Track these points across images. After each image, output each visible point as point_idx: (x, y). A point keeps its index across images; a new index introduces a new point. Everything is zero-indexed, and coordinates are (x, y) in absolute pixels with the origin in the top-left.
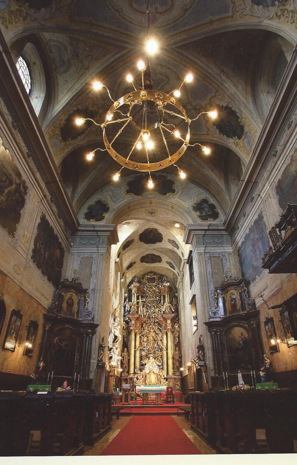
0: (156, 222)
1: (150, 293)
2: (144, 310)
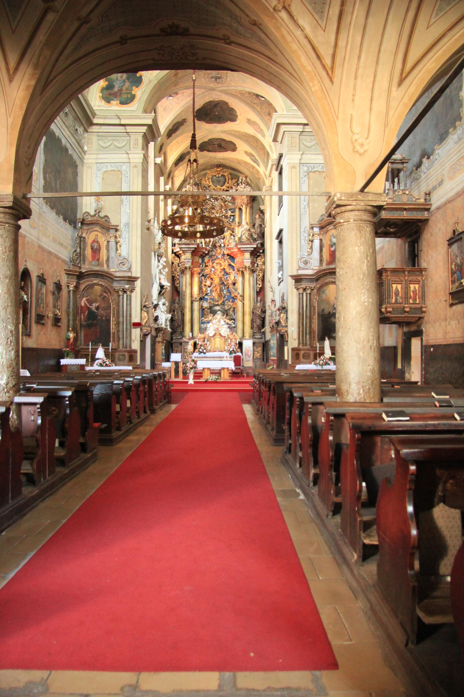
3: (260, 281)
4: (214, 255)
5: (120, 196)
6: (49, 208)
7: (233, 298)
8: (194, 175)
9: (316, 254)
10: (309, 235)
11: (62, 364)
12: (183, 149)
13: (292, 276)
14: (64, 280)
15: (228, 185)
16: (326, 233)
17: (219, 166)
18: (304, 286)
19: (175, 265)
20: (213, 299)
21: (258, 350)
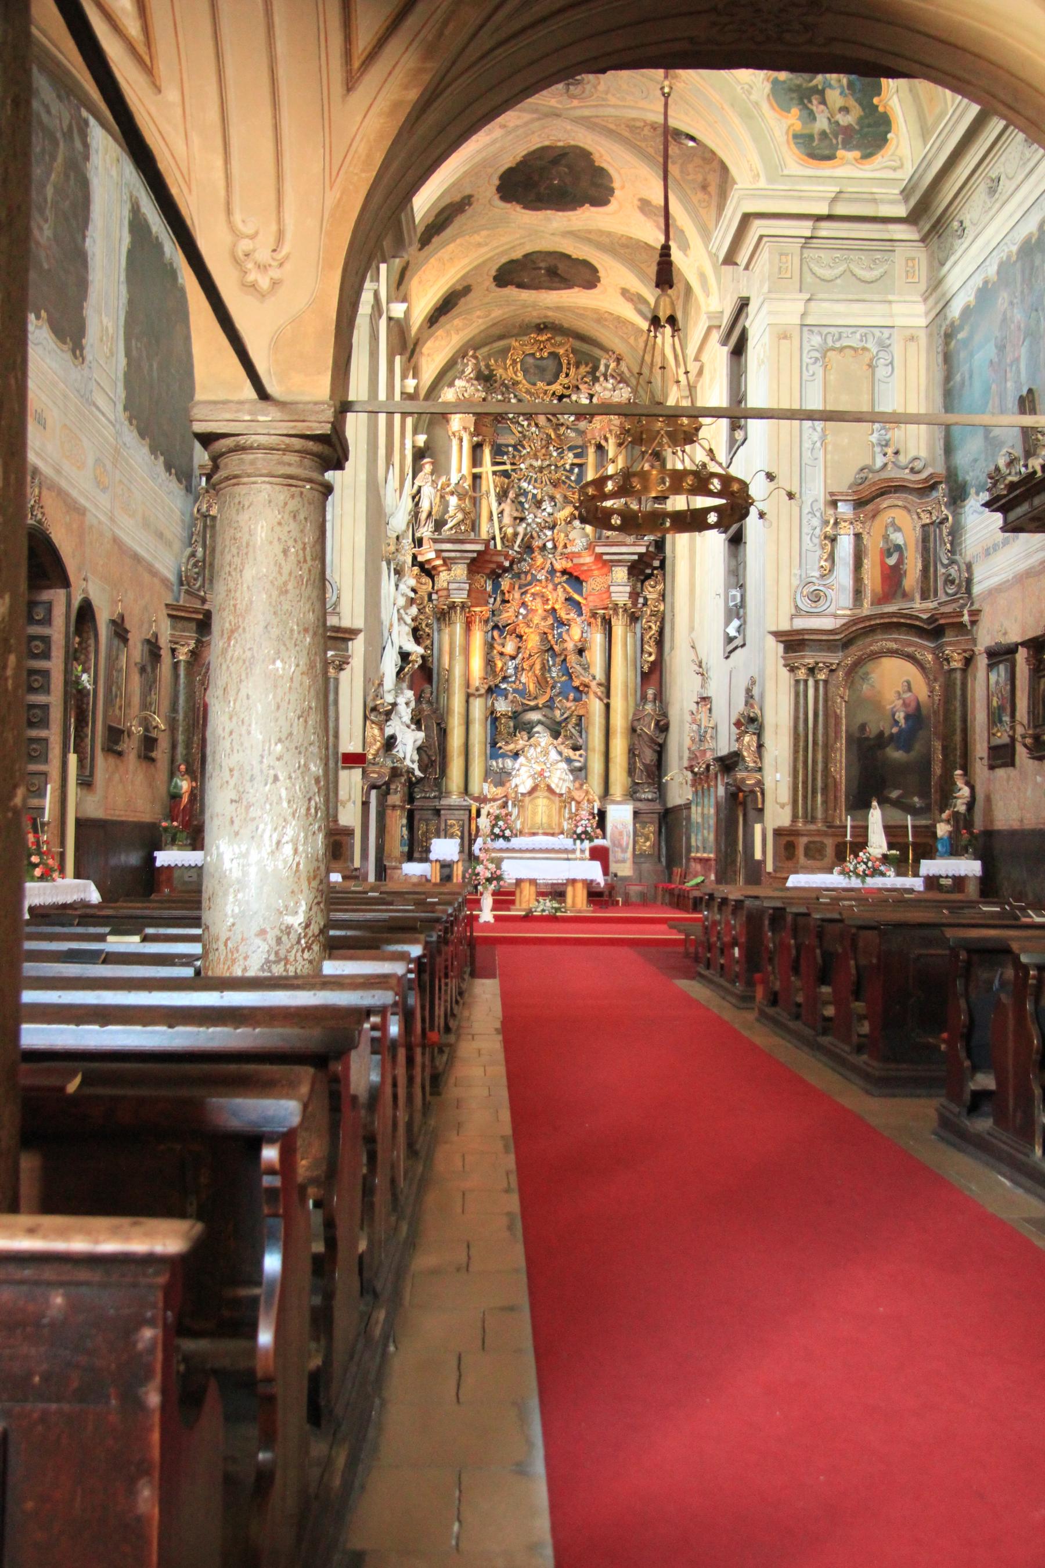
0: (589, 124)
1: (534, 429)
2: (506, 514)
3: (652, 643)
4: (526, 573)
5: (788, 421)
6: (135, 433)
7: (577, 688)
8: (475, 349)
9: (844, 575)
10: (827, 523)
11: (158, 864)
12: (454, 280)
13: (776, 634)
14: (165, 632)
15: (566, 381)
16: (874, 516)
17: (541, 328)
18: (811, 661)
19: (422, 598)
20: (522, 692)
21: (646, 831)
